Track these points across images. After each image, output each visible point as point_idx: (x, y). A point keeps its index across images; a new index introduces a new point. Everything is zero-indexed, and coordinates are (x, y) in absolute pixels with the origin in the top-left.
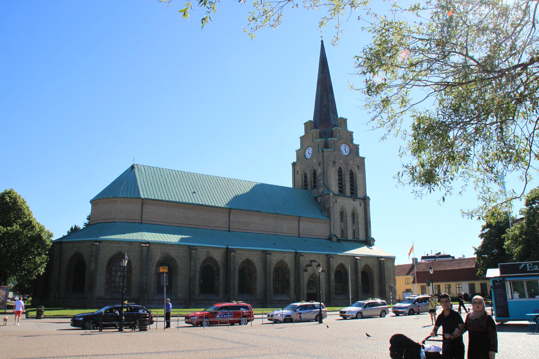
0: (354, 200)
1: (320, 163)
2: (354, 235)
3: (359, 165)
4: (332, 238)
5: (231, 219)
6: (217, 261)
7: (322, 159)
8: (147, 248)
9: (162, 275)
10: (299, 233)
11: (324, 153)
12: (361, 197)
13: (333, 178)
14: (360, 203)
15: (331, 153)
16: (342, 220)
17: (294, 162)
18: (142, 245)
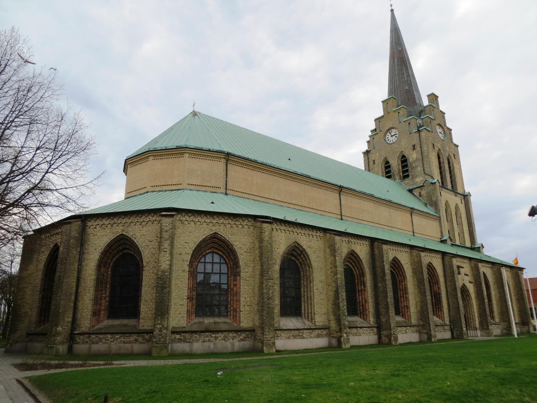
1: (414, 146)
7: (419, 141)
13: (434, 164)
14: (461, 200)
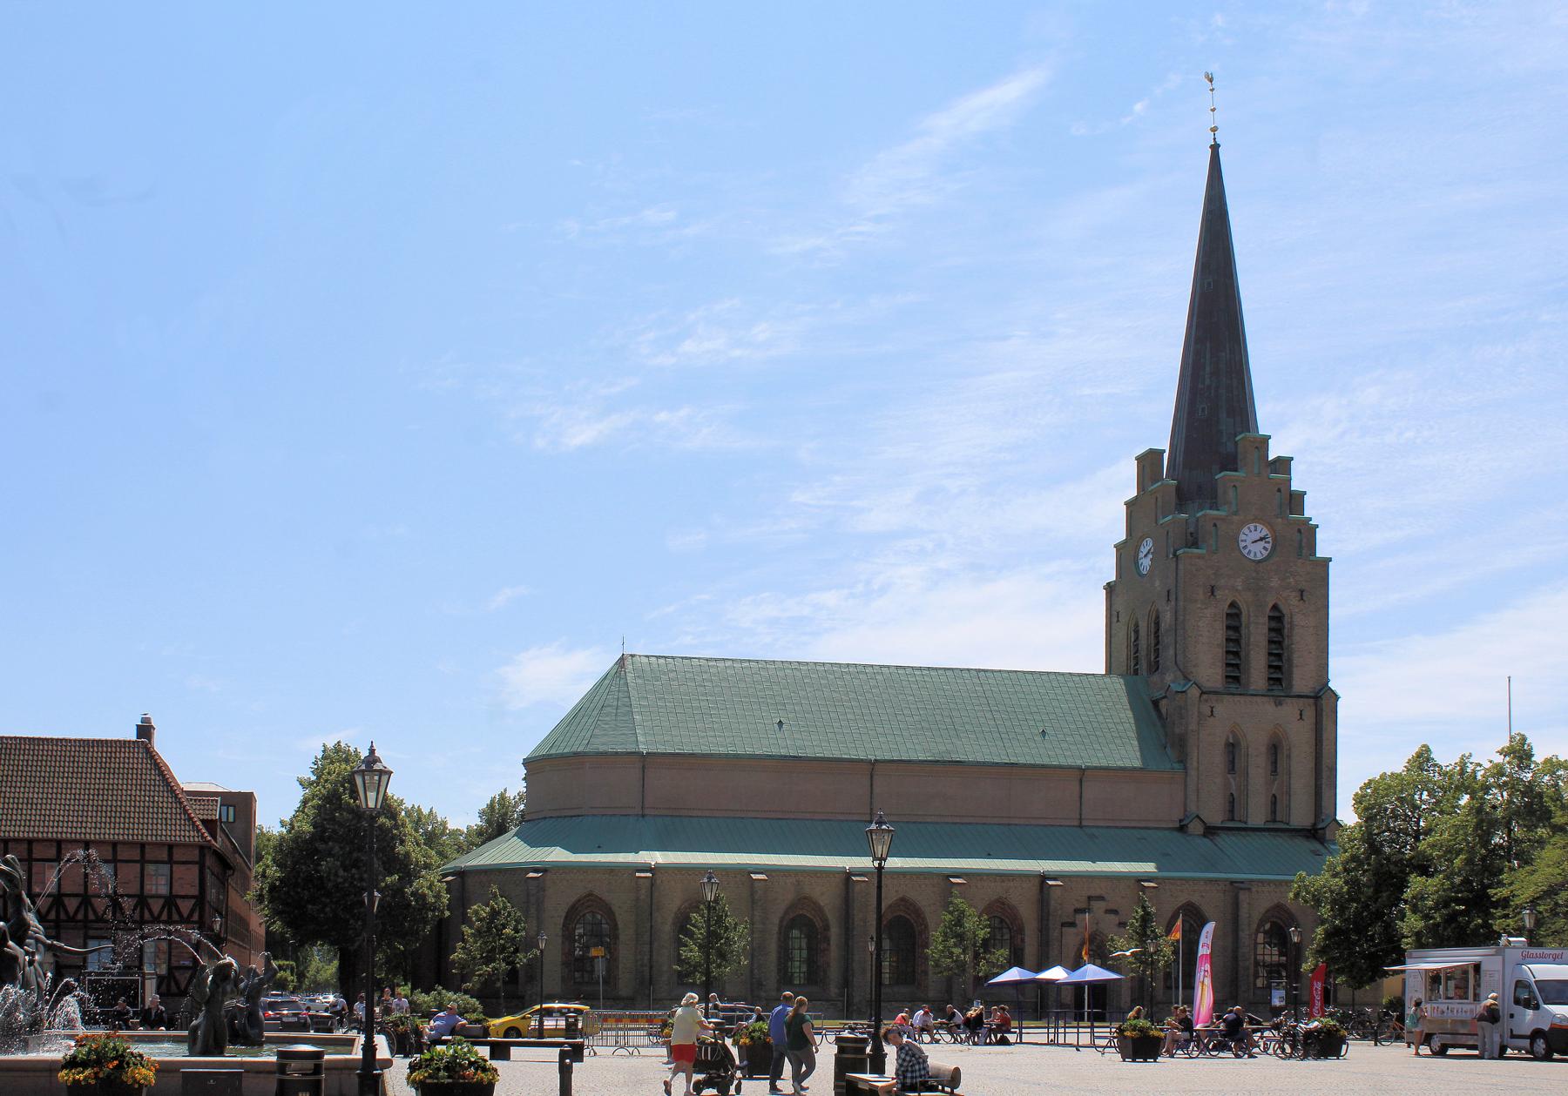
0: (1278, 704)
2: (1274, 812)
4: (1186, 825)
5: (877, 790)
6: (822, 904)
8: (648, 883)
9: (596, 960)
10: (1081, 814)
11: (1179, 562)
12: (1306, 691)
16: (1232, 767)
17: (1109, 584)
18: (637, 874)
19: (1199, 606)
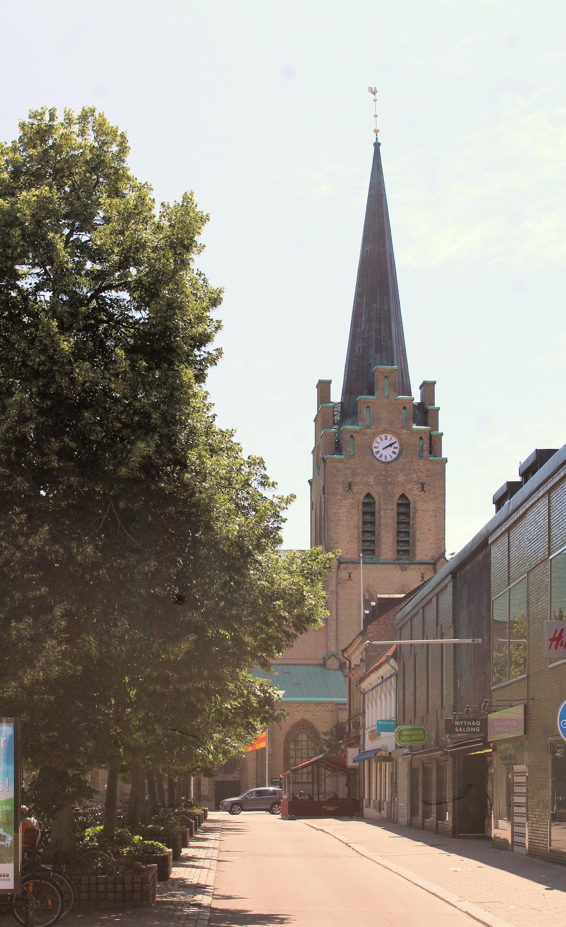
3: (424, 479)
12: (427, 559)
15: (340, 465)
19: (339, 497)
